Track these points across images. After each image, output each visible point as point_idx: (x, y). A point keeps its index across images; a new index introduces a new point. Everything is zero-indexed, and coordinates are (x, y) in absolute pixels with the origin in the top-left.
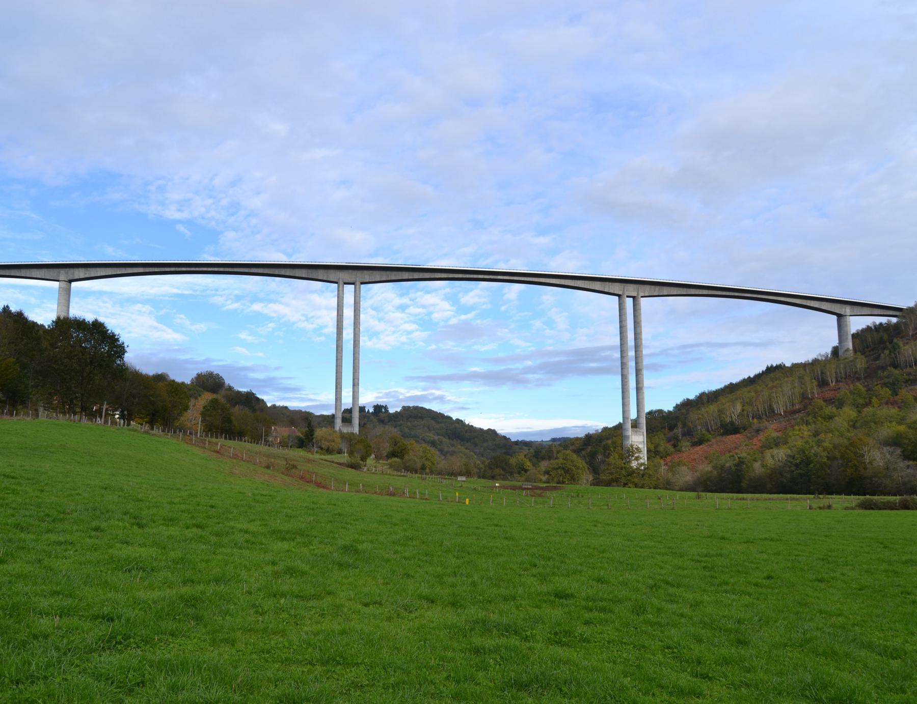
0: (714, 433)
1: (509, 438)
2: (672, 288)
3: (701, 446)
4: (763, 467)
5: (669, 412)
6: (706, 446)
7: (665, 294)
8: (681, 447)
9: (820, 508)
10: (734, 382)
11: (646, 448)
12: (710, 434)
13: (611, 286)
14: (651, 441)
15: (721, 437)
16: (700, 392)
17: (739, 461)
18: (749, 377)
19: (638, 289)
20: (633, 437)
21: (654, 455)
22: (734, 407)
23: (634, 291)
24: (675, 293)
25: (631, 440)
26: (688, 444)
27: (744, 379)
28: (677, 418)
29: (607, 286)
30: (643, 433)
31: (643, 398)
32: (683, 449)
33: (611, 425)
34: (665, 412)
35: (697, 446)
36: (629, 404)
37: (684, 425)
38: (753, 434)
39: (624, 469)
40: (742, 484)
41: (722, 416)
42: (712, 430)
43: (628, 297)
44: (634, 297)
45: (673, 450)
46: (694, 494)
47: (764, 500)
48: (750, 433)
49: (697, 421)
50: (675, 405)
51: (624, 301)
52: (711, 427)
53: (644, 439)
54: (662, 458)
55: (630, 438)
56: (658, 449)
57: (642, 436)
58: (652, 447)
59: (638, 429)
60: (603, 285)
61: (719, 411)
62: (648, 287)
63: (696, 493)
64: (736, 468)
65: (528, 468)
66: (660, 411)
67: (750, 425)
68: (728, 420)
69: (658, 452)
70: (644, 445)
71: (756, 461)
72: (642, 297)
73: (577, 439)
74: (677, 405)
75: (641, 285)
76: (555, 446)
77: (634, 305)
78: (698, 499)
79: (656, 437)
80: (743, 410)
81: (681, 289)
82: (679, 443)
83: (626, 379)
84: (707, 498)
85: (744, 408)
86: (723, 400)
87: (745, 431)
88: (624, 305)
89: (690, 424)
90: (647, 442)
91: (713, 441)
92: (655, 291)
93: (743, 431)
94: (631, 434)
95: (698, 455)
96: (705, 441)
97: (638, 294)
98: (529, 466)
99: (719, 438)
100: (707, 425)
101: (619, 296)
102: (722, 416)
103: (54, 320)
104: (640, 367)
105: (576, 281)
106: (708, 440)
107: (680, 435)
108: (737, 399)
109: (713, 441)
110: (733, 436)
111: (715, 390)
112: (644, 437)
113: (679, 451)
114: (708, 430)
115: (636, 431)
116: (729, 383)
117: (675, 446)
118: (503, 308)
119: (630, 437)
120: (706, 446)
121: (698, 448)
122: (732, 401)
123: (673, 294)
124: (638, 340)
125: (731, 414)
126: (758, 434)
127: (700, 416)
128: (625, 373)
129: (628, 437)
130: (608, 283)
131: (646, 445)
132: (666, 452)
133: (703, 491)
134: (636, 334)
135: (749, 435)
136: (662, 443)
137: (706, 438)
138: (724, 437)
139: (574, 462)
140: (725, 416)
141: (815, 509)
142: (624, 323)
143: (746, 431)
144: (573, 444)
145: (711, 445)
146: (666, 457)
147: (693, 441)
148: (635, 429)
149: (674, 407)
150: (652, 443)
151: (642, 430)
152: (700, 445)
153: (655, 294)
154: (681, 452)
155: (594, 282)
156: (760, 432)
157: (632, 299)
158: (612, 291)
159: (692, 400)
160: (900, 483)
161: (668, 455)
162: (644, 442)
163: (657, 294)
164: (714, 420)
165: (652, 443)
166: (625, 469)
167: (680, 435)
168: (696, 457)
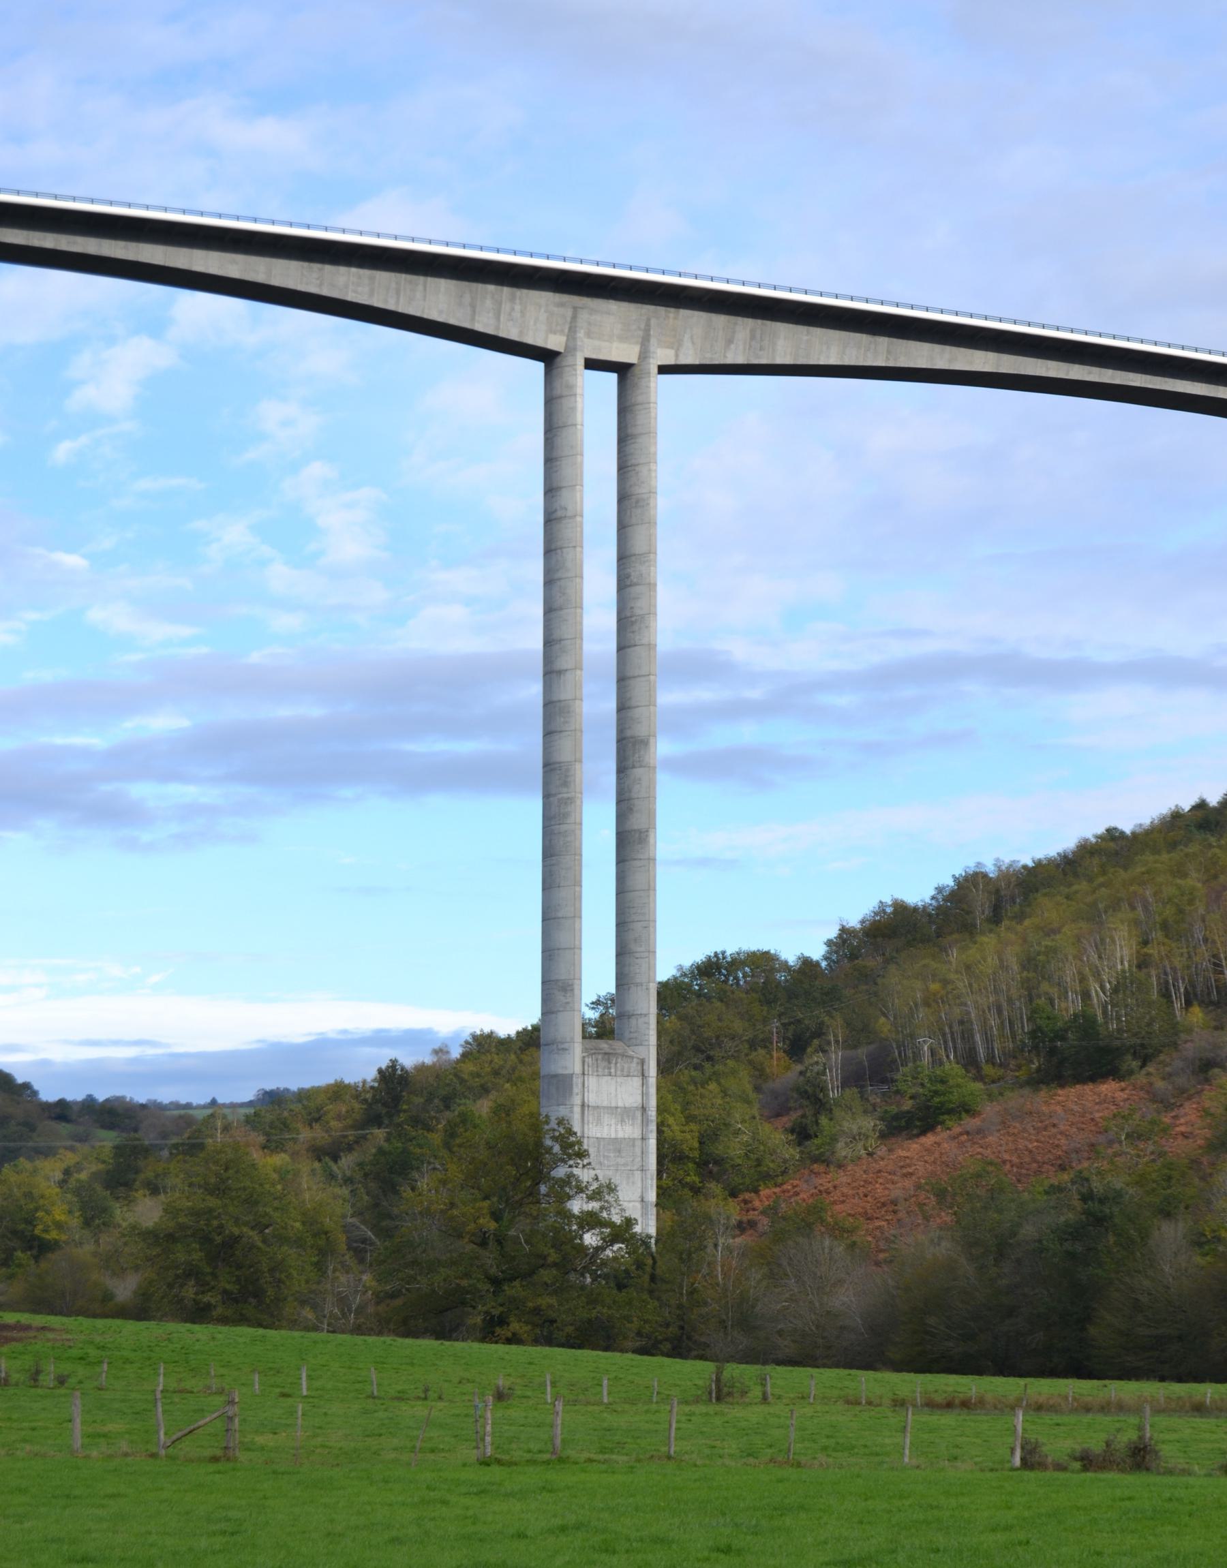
0: (1001, 1072)
1: (27, 1086)
2: (818, 332)
3: (929, 1139)
4: (1200, 1245)
5: (807, 965)
6: (954, 1138)
7: (779, 360)
8: (834, 1139)
9: (1088, 1461)
10: (1127, 828)
11: (652, 1143)
12: (979, 1077)
13: (506, 307)
14: (686, 1105)
15: (1026, 1091)
16: (959, 871)
17: (1087, 1213)
18: (1201, 806)
19: (648, 325)
20: (592, 1082)
21: (693, 1178)
22: (1100, 946)
23: (622, 339)
24: (833, 360)
25: (577, 1100)
26: (868, 1124)
27: (1176, 816)
28: (831, 997)
29: (489, 303)
30: (642, 1062)
31: (650, 888)
32: (842, 1150)
33: (507, 1027)
34: (785, 965)
35: (911, 1137)
36: (577, 916)
37: (859, 1032)
38: (1181, 1081)
39: (492, 1244)
40: (1092, 1331)
41: (1045, 987)
42: (991, 1059)
43: (591, 364)
44: (622, 369)
45: (792, 1153)
46: (696, 1372)
47: (1074, 1410)
48: (1167, 1077)
49: (922, 1013)
50: (833, 933)
51: (571, 387)
52: (988, 1040)
53: (644, 1095)
54: (733, 1194)
55: (577, 1089)
56: (719, 1149)
57: (637, 1081)
58: (689, 1140)
59: (618, 1046)
60: (467, 299)
61: (1029, 963)
62: (695, 320)
63: (709, 1367)
64: (1068, 1246)
65: (53, 1235)
66: (762, 961)
67: (1174, 1035)
68: (1071, 1006)
69: (718, 1162)
70: (645, 1122)
71: (1168, 1215)
72: (664, 370)
73: (338, 1091)
74: (843, 930)
75: (661, 310)
76: (226, 1129)
77: (625, 409)
78: (718, 1399)
79: (713, 1086)
80: (1143, 963)
81: (863, 338)
82: (824, 1121)
83: (566, 784)
84: (765, 1398)
85: (1148, 950)
86: (1048, 909)
87: (1143, 1066)
88: (574, 409)
89: (883, 1026)
90: (661, 1110)
91: (990, 1110)
92: (730, 341)
93: (1135, 1064)
94: (578, 1069)
95: (909, 1183)
96: (950, 1112)
97: (644, 355)
98: (59, 1226)
99: (1016, 1099)
100: (967, 1036)
101: (547, 357)
102: (1045, 987)
103: (384, 1067)
104: (640, 731)
105: (328, 269)
106: (966, 1109)
107: (832, 1080)
108: (1115, 905)
109: (990, 1110)
110: (1088, 1088)
111: (1030, 864)
112: (644, 1084)
113: (816, 1160)
114: (970, 1061)
115: (608, 1056)
116: (1101, 830)
117: (802, 1134)
118: (63, 451)
119: (577, 1081)
120: (954, 1138)
121: (912, 1149)
122: (1094, 916)
123: (823, 361)
124: (635, 590)
125: (1083, 979)
126: (1207, 1081)
127: (935, 987)
128: (564, 753)
129: (563, 1084)
130: (491, 288)
131: (653, 1127)
132: (759, 1162)
133: (749, 1357)
134: (624, 558)
135: (1160, 1085)
136: (739, 1113)
137: (955, 1097)
138: (1043, 1093)
139: (256, 1203)
140: (1054, 992)
141: (1060, 1467)
142: (564, 497)
143: (1150, 1068)
144: (315, 1118)
145: (979, 1131)
146: (756, 1191)
147: (893, 1109)
148: (604, 1045)
149: (829, 943)
150: (690, 1119)
151: (640, 1052)
152: (923, 1132)
153: (730, 359)
154: (827, 1163)
155: (421, 279)
156: (1216, 1070)
157: (613, 377)
158: (511, 332)
159: (915, 909)
160: (1190, 861)
161: (767, 1177)
162: (644, 1109)
163: (740, 360)
164: (1000, 1011)
165: (690, 1119)
166: (499, 1242)
167: (832, 1080)
168: (896, 1193)
